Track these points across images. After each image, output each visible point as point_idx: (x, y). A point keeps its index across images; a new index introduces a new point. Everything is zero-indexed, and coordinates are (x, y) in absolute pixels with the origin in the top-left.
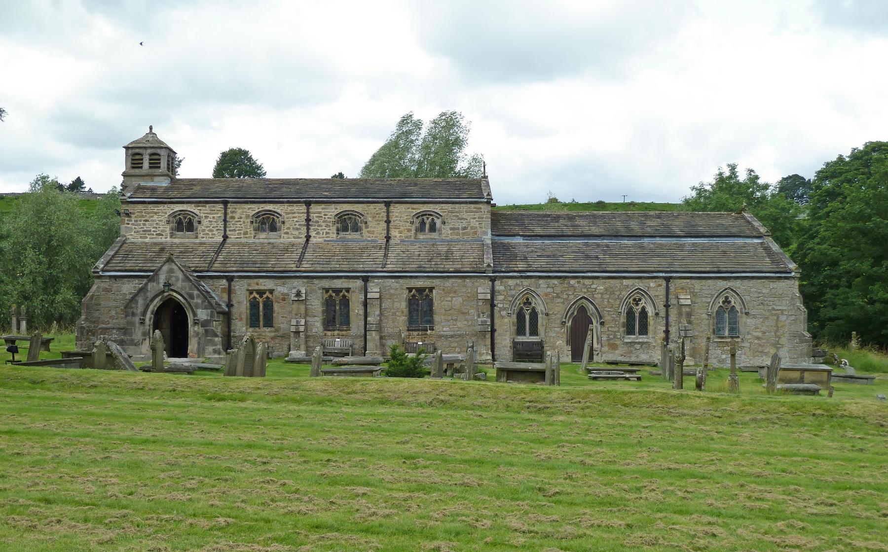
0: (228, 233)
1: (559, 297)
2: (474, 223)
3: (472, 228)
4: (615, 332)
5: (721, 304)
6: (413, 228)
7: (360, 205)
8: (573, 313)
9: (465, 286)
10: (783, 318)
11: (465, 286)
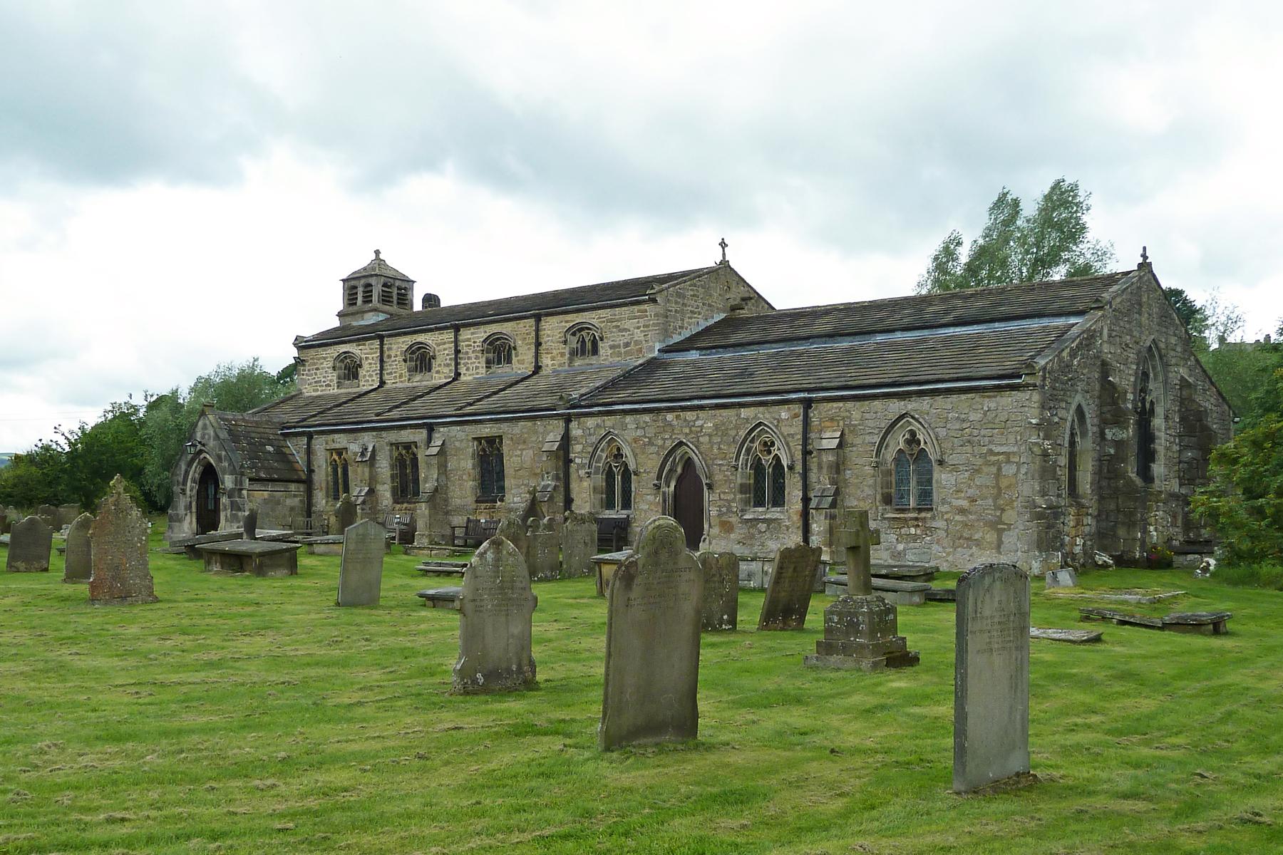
0: (386, 377)
1: (653, 445)
2: (638, 335)
3: (637, 343)
4: (729, 501)
5: (901, 446)
6: (567, 351)
7: (510, 324)
8: (671, 471)
9: (536, 432)
10: (1009, 470)
11: (536, 432)
